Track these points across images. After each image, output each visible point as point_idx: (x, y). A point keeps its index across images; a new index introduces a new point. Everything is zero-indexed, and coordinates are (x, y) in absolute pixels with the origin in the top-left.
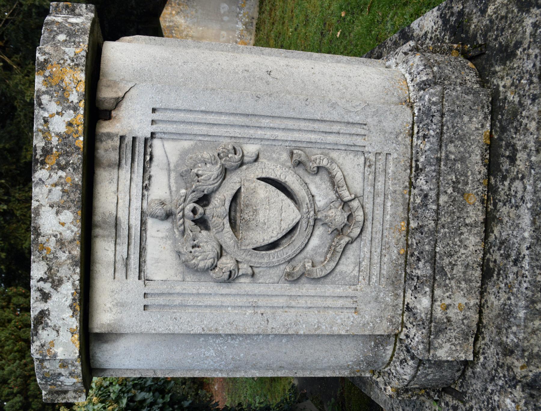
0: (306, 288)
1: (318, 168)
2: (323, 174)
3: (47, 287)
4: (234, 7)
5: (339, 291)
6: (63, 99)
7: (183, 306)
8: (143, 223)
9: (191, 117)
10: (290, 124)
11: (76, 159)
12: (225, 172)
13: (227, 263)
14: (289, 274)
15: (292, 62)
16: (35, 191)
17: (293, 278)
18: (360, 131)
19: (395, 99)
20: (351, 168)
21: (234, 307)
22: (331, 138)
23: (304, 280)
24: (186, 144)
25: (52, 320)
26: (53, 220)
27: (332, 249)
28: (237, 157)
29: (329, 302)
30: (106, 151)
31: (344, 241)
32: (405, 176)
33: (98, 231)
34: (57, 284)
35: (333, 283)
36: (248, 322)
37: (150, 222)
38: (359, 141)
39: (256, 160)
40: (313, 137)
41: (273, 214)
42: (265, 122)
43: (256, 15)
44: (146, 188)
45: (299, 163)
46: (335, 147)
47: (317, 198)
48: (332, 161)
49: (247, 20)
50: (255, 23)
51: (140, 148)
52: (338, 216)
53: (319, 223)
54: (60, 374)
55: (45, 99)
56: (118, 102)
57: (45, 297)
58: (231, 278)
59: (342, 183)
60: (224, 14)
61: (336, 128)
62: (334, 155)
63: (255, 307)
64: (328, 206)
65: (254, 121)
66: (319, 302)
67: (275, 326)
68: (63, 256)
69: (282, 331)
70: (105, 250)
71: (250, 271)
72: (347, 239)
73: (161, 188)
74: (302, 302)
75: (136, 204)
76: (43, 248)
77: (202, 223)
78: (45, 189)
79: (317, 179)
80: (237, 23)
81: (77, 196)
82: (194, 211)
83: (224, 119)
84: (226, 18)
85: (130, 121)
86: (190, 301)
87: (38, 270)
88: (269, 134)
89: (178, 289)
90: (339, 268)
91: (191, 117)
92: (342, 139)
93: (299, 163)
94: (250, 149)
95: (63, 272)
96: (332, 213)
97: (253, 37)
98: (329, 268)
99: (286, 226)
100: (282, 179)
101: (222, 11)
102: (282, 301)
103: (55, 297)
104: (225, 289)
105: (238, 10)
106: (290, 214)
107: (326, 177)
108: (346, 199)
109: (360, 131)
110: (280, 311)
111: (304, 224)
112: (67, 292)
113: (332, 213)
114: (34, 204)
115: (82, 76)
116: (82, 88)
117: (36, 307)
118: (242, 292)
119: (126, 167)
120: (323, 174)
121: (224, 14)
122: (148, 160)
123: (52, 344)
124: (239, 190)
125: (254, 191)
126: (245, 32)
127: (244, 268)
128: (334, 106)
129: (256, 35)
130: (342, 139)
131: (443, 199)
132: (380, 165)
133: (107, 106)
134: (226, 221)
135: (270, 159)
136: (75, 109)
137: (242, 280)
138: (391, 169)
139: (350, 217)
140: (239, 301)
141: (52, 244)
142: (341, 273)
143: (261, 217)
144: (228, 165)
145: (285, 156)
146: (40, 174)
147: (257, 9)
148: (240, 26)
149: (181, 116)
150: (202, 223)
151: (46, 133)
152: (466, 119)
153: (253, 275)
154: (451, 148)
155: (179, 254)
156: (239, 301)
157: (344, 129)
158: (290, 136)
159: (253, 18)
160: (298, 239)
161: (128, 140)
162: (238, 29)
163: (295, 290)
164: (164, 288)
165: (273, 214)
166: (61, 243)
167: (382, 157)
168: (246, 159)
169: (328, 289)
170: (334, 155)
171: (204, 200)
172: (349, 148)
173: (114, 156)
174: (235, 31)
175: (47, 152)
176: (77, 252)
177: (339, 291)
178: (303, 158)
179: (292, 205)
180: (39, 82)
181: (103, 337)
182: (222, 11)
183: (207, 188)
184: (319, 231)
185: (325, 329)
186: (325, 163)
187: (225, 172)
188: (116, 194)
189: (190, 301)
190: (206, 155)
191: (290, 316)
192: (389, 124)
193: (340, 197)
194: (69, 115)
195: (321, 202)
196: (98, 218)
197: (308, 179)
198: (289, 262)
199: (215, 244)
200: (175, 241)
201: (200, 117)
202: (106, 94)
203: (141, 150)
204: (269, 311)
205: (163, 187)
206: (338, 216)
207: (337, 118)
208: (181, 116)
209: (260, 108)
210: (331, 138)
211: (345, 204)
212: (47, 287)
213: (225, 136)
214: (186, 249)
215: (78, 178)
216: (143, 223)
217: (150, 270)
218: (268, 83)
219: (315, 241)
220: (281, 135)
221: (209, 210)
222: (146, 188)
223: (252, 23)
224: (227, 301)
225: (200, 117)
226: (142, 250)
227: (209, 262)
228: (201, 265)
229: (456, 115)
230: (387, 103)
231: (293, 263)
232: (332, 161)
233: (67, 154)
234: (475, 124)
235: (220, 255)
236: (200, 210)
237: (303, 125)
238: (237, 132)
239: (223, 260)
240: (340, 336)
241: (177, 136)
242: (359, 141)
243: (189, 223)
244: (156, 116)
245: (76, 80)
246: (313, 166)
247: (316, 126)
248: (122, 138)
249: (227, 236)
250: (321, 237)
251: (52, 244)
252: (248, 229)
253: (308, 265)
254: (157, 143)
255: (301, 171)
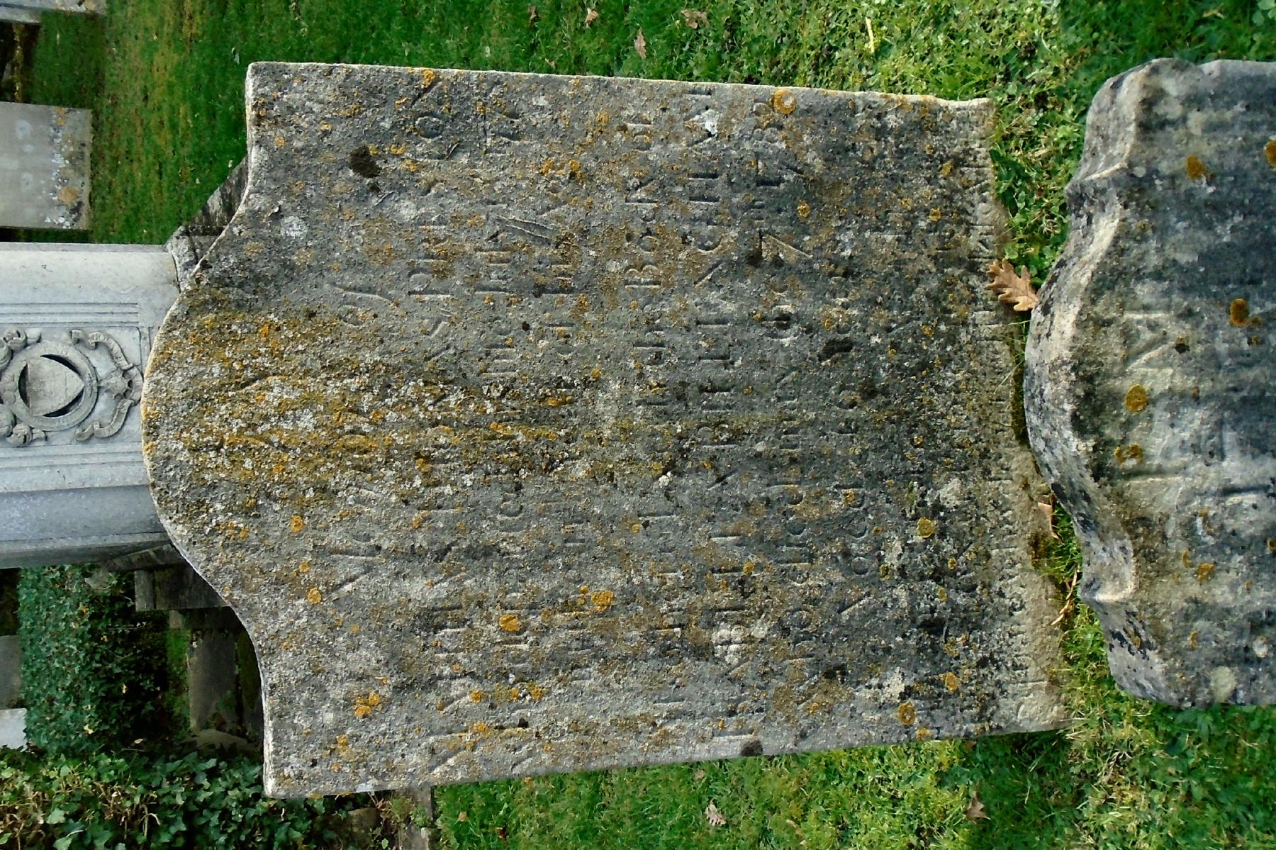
0: (98, 447)
1: (97, 344)
4: (43, 127)
5: (128, 447)
10: (67, 309)
12: (12, 353)
13: (21, 429)
14: (80, 436)
15: (66, 255)
17: (87, 439)
18: (132, 309)
19: (164, 280)
20: (128, 341)
21: (31, 468)
23: (94, 440)
27: (117, 412)
28: (21, 339)
29: (120, 458)
31: (128, 403)
35: (122, 441)
36: (47, 480)
38: (133, 318)
39: (39, 341)
40: (89, 318)
41: (58, 385)
42: (43, 309)
43: (88, 139)
45: (78, 341)
46: (111, 325)
47: (98, 369)
49: (72, 149)
50: (88, 154)
52: (119, 383)
53: (102, 391)
58: (26, 442)
59: (120, 354)
60: (23, 142)
61: (109, 309)
62: (111, 331)
63: (52, 466)
64: (109, 376)
66: (110, 459)
67: (73, 480)
69: (79, 485)
71: (43, 435)
72: (129, 402)
74: (94, 460)
79: (97, 352)
80: (52, 156)
84: (29, 148)
88: (48, 319)
90: (125, 428)
92: (115, 318)
93: (78, 341)
94: (33, 333)
96: (113, 381)
97: (87, 180)
98: (116, 429)
99: (72, 394)
100: (63, 354)
101: (20, 135)
102: (75, 460)
104: (21, 453)
105: (52, 131)
106: (74, 384)
107: (105, 351)
108: (125, 368)
109: (132, 309)
110: (75, 469)
111: (88, 391)
113: (113, 381)
118: (38, 453)
120: (101, 347)
121: (23, 142)
124: (26, 368)
126: (70, 171)
127: (38, 433)
128: (105, 290)
129: (92, 178)
130: (115, 318)
134: (17, 393)
135: (52, 339)
137: (37, 444)
139: (130, 383)
140: (36, 462)
142: (128, 432)
143: (48, 387)
145: (65, 336)
147: (89, 128)
148: (60, 161)
153: (46, 438)
156: (36, 462)
157: (116, 309)
158: (68, 319)
159: (84, 145)
160: (85, 405)
162: (55, 166)
163: (86, 449)
165: (58, 385)
168: (29, 341)
169: (118, 447)
170: (111, 331)
174: (50, 172)
177: (128, 447)
178: (81, 336)
179: (75, 375)
182: (20, 135)
184: (104, 397)
185: (119, 482)
186: (101, 338)
187: (12, 353)
191: (85, 471)
193: (119, 367)
195: (102, 373)
198: (79, 425)
199: (8, 413)
204: (65, 470)
206: (119, 383)
207: (109, 301)
211: (125, 372)
218: (44, 276)
219: (101, 406)
220: (59, 319)
223: (82, 153)
224: (25, 463)
230: (156, 284)
231: (83, 426)
232: (109, 336)
235: (14, 424)
237: (78, 309)
238: (19, 319)
239: (18, 426)
240: (135, 487)
242: (133, 318)
246: (91, 342)
247: (90, 308)
250: (106, 402)
252: (38, 398)
253: (96, 427)
255: (80, 347)
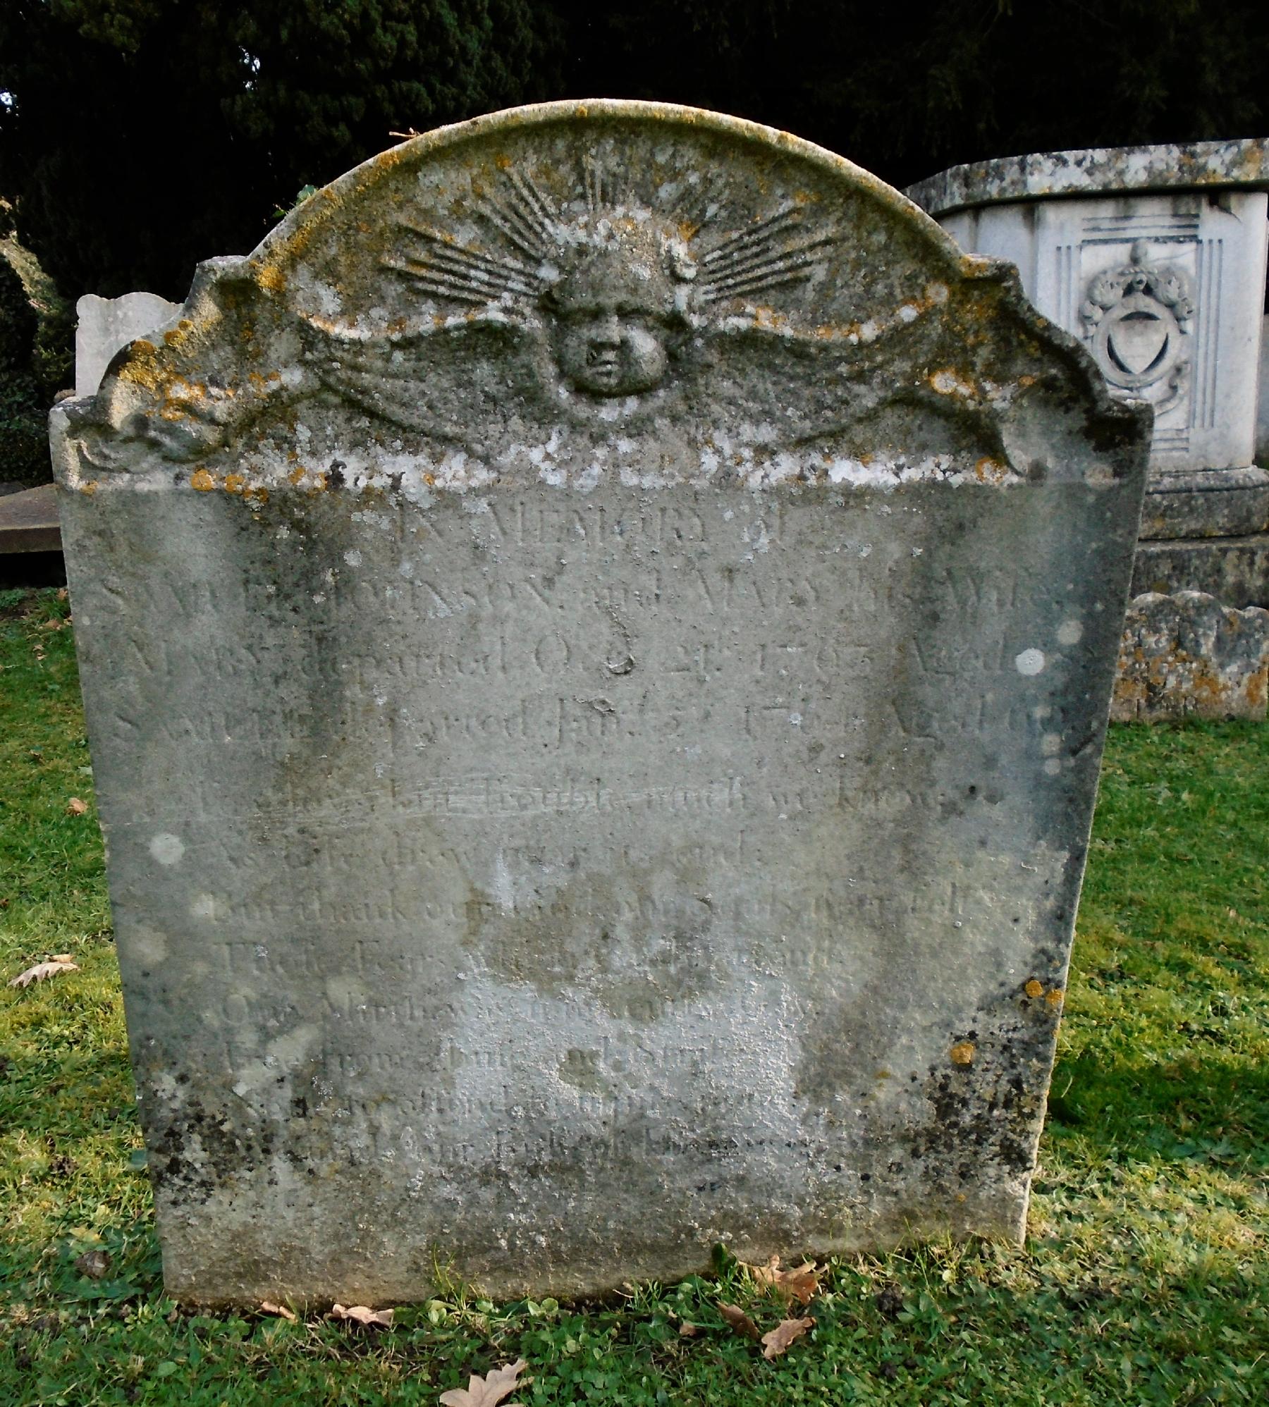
2: (1170, 392)
3: (1087, 164)
6: (1235, 164)
7: (1059, 281)
8: (1127, 241)
9: (1215, 272)
11: (1187, 178)
13: (1098, 314)
16: (1163, 147)
22: (1199, 397)
24: (1192, 271)
25: (1061, 171)
26: (1139, 165)
28: (1185, 314)
30: (1187, 205)
32: (1170, 467)
33: (1122, 202)
34: (1089, 172)
37: (1129, 246)
38: (1198, 422)
40: (1200, 379)
42: (1212, 336)
44: (1157, 240)
46: (1192, 401)
48: (1182, 399)
51: (1189, 232)
54: (1002, 179)
55: (1234, 149)
56: (1226, 210)
57: (1079, 163)
62: (1186, 401)
65: (1212, 324)
68: (1111, 175)
70: (1107, 210)
73: (1157, 255)
75: (1144, 233)
76: (1117, 157)
77: (1129, 290)
78: (1164, 156)
79: (1166, 387)
81: (1159, 182)
82: (1140, 282)
83: (1213, 301)
85: (1212, 223)
86: (1064, 286)
87: (1100, 155)
88: (1202, 340)
89: (1074, 275)
91: (1215, 272)
95: (1099, 177)
99: (1128, 363)
103: (1079, 170)
104: (1073, 315)
112: (1082, 180)
114: (1152, 148)
115: (1252, 178)
116: (1243, 179)
117: (1070, 155)
119: (1175, 222)
122: (1178, 240)
123: (1041, 171)
125: (1157, 331)
128: (1228, 396)
131: (1158, 497)
132: (1178, 444)
133: (1222, 201)
136: (1227, 175)
138: (1175, 454)
141: (1120, 165)
143: (1137, 340)
144: (1178, 307)
145: (1184, 357)
146: (1176, 151)
149: (1215, 264)
150: (1129, 290)
151: (1207, 153)
152: (1226, 512)
154: (1201, 501)
155: (1105, 272)
157: (1208, 406)
161: (1195, 221)
164: (1074, 262)
166: (1121, 173)
167: (1184, 445)
170: (1186, 401)
171: (1148, 291)
172: (1192, 415)
173: (1183, 210)
175: (1193, 155)
176: (1114, 186)
180: (1247, 143)
181: (976, 218)
183: (1159, 292)
187: (1171, 306)
188: (1152, 218)
189: (1064, 286)
190: (1186, 288)
192: (1213, 447)
194: (1221, 171)
196: (1132, 201)
197: (1165, 380)
200: (1113, 269)
201: (1215, 281)
202: (1233, 201)
203: (1188, 233)
205: (1157, 255)
208: (1215, 264)
209: (1223, 331)
210: (1199, 397)
212: (1087, 164)
213: (1201, 303)
214: (1110, 277)
215: (1172, 182)
216: (1127, 241)
217: (1089, 251)
220: (1201, 352)
221: (1140, 295)
222: (1157, 240)
225: (1215, 281)
226: (1106, 242)
227: (1099, 298)
228: (1097, 292)
229: (1229, 502)
233: (1191, 172)
234: (1222, 521)
236: (1142, 287)
241: (1199, 262)
243: (1129, 279)
244: (1215, 243)
245: (1248, 174)
246: (1177, 382)
247: (1210, 382)
248: (1197, 216)
249: (1119, 312)
251: (1120, 165)
254: (1193, 245)
255: (1173, 372)
